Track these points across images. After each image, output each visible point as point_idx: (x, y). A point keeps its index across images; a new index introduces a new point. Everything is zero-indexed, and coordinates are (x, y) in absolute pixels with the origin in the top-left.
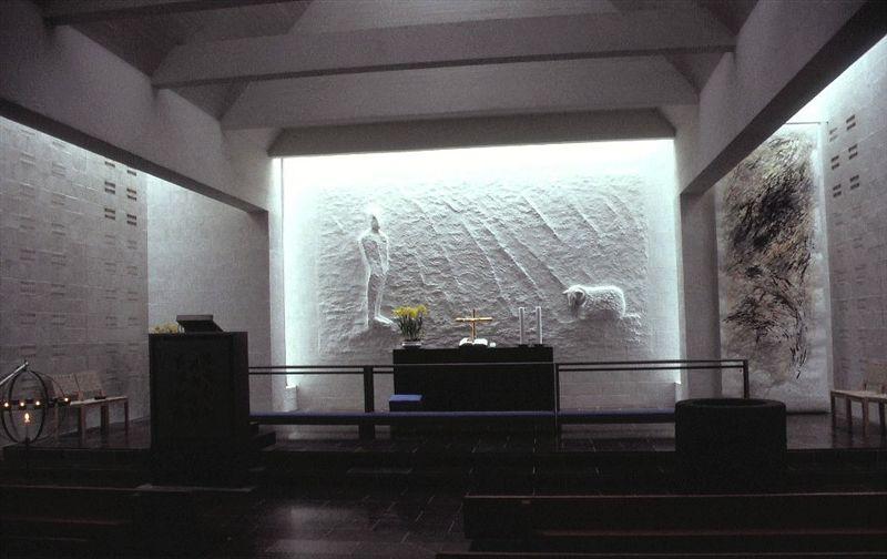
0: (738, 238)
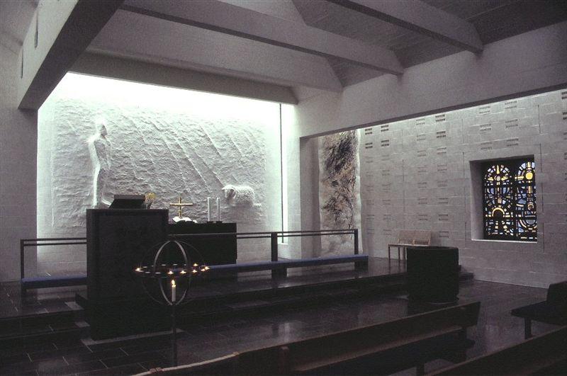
0: (328, 164)
